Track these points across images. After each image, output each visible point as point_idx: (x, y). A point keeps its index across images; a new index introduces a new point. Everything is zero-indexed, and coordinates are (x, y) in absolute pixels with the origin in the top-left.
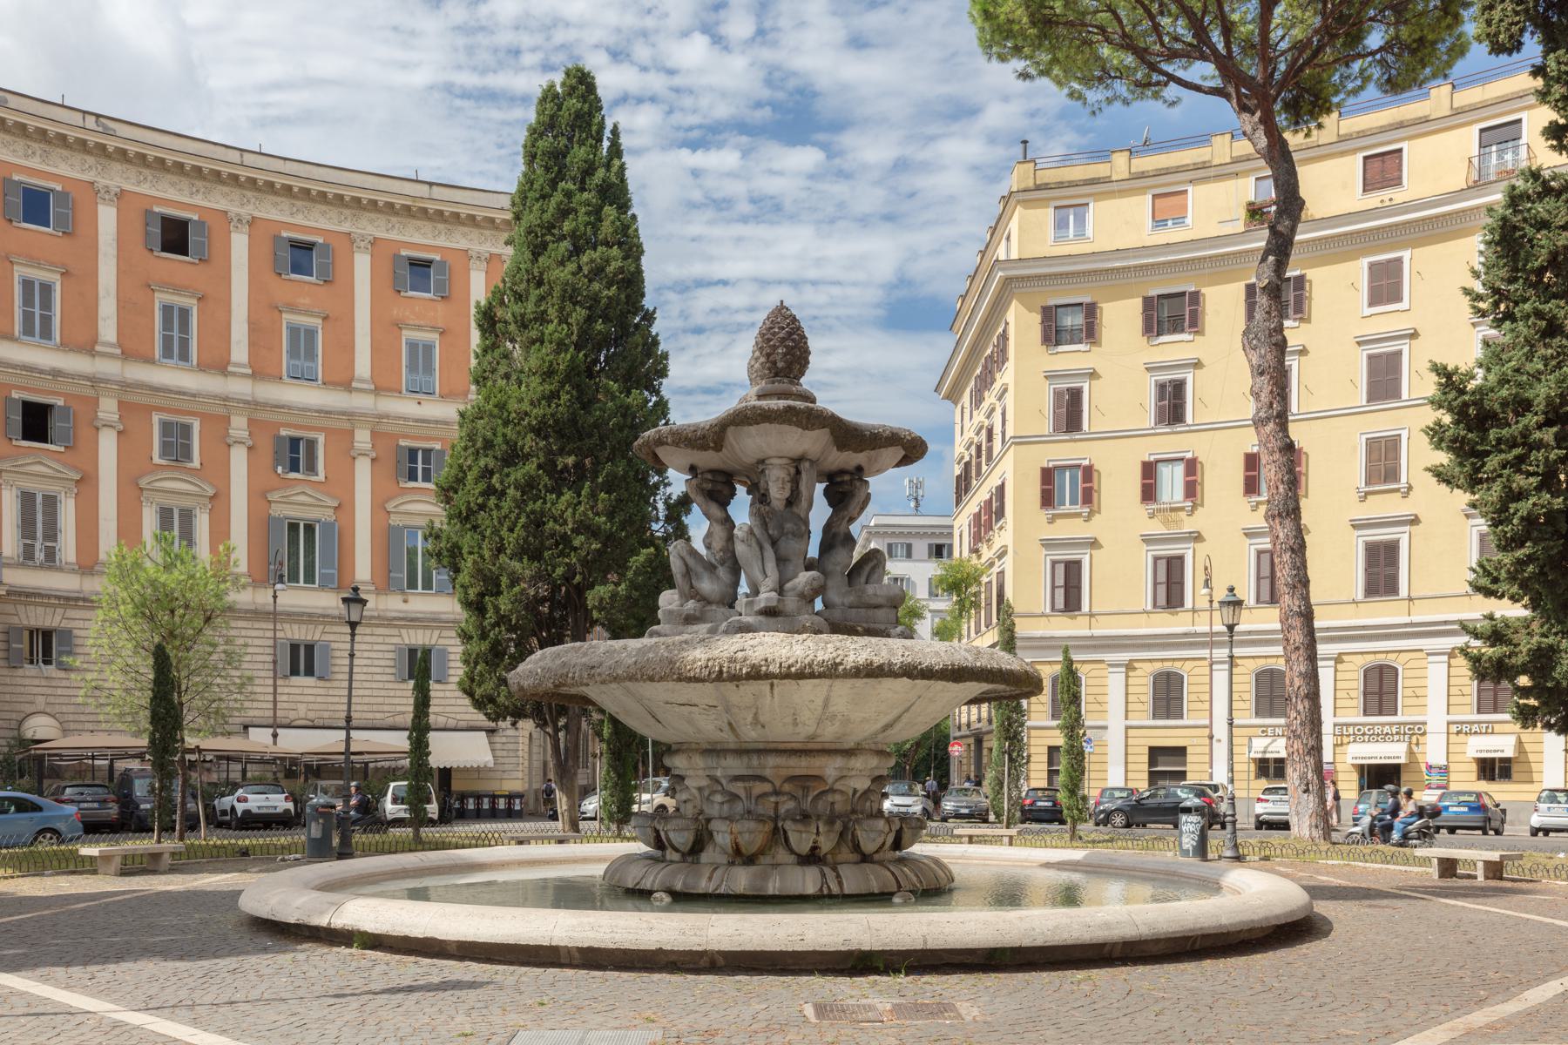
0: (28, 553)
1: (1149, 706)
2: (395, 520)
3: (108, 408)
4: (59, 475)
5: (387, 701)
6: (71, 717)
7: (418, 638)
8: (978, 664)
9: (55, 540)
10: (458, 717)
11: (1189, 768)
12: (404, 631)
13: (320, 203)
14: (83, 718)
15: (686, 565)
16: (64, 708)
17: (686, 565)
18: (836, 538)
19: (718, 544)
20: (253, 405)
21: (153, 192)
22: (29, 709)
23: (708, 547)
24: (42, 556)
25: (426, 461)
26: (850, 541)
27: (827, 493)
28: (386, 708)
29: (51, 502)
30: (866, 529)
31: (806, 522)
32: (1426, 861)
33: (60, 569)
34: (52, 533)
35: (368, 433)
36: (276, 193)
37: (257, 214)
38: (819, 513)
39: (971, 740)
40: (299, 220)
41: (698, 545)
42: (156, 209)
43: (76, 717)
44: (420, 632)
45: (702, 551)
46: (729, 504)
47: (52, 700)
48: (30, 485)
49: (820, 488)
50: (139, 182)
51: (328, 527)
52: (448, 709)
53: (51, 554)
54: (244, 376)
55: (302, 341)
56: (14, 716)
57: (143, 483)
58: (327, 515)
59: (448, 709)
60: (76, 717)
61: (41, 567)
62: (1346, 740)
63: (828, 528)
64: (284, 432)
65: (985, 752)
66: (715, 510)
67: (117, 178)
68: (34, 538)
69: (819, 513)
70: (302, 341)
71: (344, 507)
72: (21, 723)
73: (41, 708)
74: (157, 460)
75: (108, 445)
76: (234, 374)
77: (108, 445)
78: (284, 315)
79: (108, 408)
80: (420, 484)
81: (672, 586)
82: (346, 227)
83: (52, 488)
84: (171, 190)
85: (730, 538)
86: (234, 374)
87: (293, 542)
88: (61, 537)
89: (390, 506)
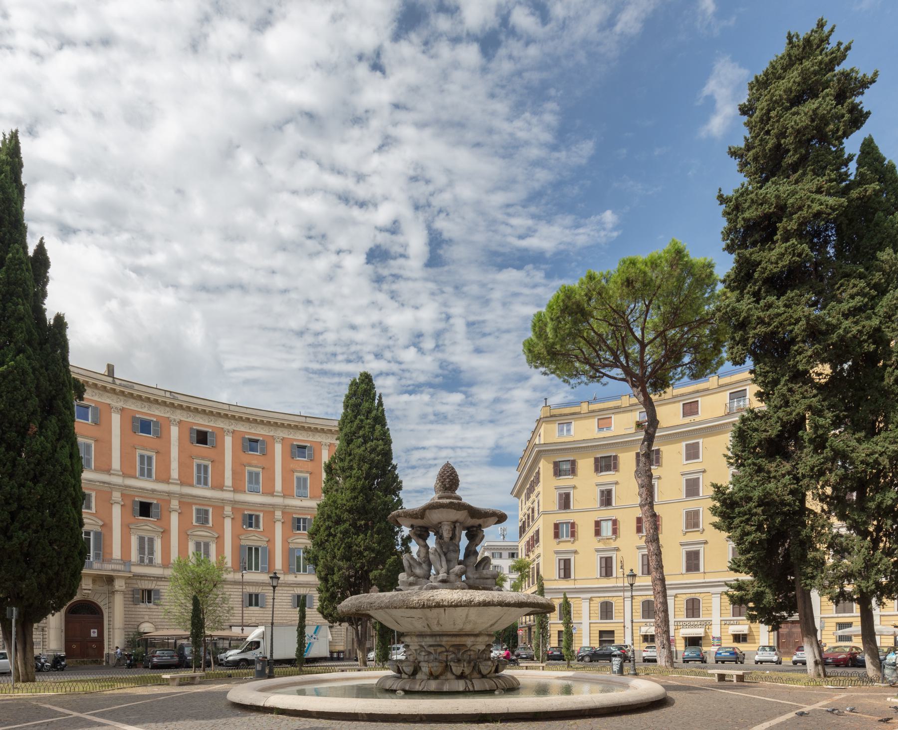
0: (142, 560)
2: (291, 546)
3: (175, 504)
7: (301, 591)
11: (615, 639)
12: (295, 589)
14: (164, 624)
18: (471, 552)
19: (422, 555)
20: (182, 495)
22: (142, 620)
23: (419, 556)
27: (467, 535)
29: (151, 541)
30: (482, 551)
31: (458, 546)
33: (155, 566)
34: (151, 552)
38: (464, 542)
39: (527, 629)
40: (252, 431)
44: (302, 589)
45: (415, 556)
48: (143, 534)
49: (464, 533)
51: (264, 549)
53: (151, 560)
58: (264, 544)
61: (147, 565)
63: (467, 548)
66: (421, 542)
69: (464, 542)
70: (254, 478)
71: (271, 541)
72: (138, 626)
75: (174, 519)
77: (174, 519)
79: (175, 504)
81: (404, 571)
82: (271, 434)
83: (151, 535)
85: (427, 553)
88: (155, 554)
89: (290, 540)
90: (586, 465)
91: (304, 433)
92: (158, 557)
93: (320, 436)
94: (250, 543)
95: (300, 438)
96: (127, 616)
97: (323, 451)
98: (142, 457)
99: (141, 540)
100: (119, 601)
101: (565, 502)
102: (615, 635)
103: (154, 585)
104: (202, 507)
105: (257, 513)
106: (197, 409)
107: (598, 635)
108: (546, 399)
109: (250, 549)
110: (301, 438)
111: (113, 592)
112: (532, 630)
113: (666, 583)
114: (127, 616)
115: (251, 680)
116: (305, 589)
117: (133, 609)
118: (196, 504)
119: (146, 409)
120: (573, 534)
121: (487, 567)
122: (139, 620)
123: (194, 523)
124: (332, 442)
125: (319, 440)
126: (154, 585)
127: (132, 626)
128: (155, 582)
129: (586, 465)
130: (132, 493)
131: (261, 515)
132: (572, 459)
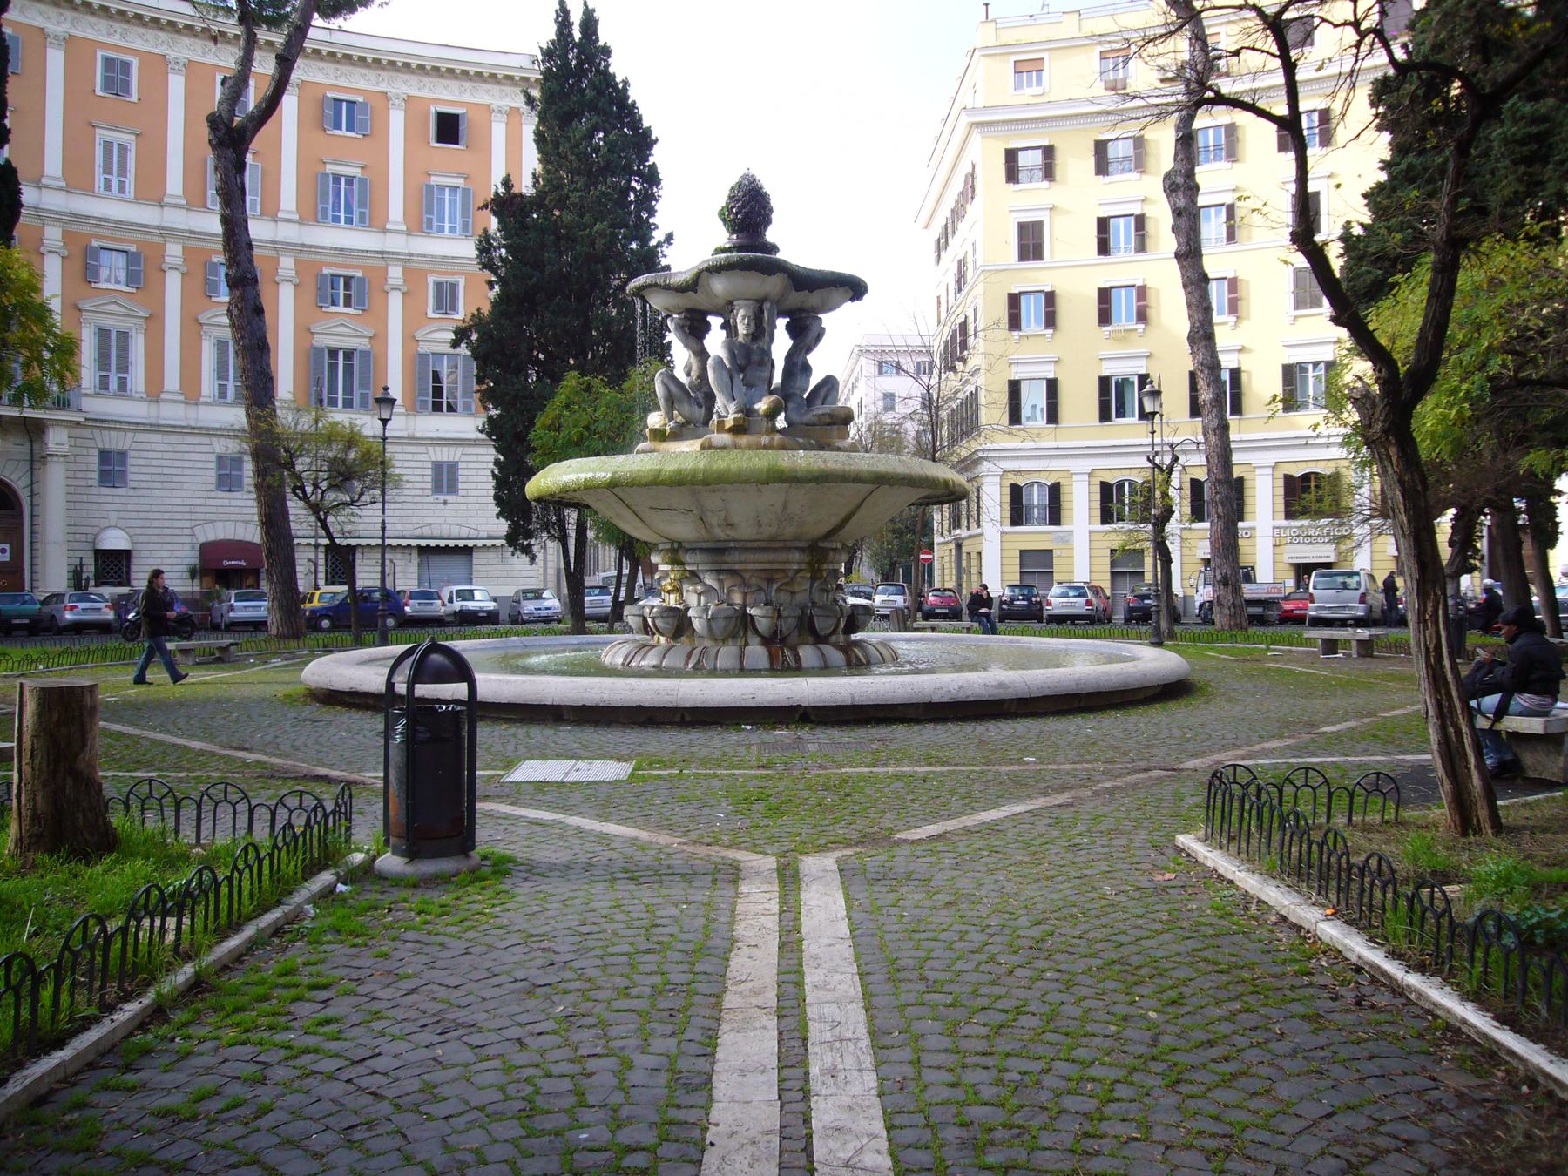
0: (104, 383)
1: (1283, 515)
2: (424, 348)
3: (395, 274)
4: (352, 332)
5: (416, 513)
6: (139, 531)
7: (445, 455)
8: (715, 467)
9: (127, 372)
10: (480, 528)
11: (1055, 569)
12: (430, 449)
13: (361, 67)
14: (150, 531)
15: (669, 391)
16: (133, 523)
17: (669, 391)
18: (797, 366)
19: (694, 373)
20: (302, 248)
21: (215, 62)
22: (104, 523)
23: (688, 374)
24: (115, 387)
25: (347, 286)
26: (807, 369)
27: (789, 328)
28: (415, 520)
29: (124, 337)
30: (821, 363)
31: (768, 353)
32: (1310, 642)
33: (131, 398)
34: (124, 366)
35: (180, 247)
36: (144, 25)
37: (74, 32)
38: (781, 344)
39: (952, 546)
40: (342, 82)
41: (680, 374)
42: (329, 95)
43: (143, 531)
44: (445, 449)
45: (684, 379)
46: (704, 337)
47: (122, 515)
48: (106, 322)
49: (782, 323)
50: (109, 34)
51: (365, 355)
52: (470, 520)
53: (122, 384)
54: (60, 189)
55: (115, 158)
56: (89, 530)
57: (203, 318)
58: (360, 344)
59: (470, 520)
60: (143, 531)
61: (115, 396)
62: (1284, 541)
63: (790, 358)
64: (326, 271)
65: (964, 556)
66: (693, 342)
67: (402, 86)
68: (109, 370)
69: (781, 344)
70: (115, 158)
71: (379, 337)
72: (96, 536)
73: (113, 522)
74: (431, 314)
75: (395, 303)
76: (169, 205)
77: (395, 303)
78: (98, 131)
79: (395, 274)
80: (341, 309)
81: (657, 408)
82: (382, 88)
83: (123, 324)
84: (139, 41)
85: (703, 369)
86: (169, 205)
87: (333, 368)
88: (132, 369)
89: (419, 335)
90: (1076, 163)
91: (453, 84)
92: (138, 378)
93: (487, 91)
94: (334, 342)
95: (445, 96)
96: (72, 513)
97: (495, 125)
98: (108, 146)
99: (103, 334)
100: (55, 478)
101: (1031, 243)
102: (1055, 561)
103: (128, 441)
104: (443, 279)
105: (451, 279)
106: (479, 74)
107: (1108, 560)
108: (987, 5)
109: (333, 353)
110: (450, 96)
111: (43, 457)
112: (965, 550)
113: (1232, 437)
114: (72, 513)
115: (320, 656)
116: (452, 449)
117: (85, 498)
118: (433, 272)
119: (468, 94)
120: (1051, 321)
121: (829, 399)
122: (95, 522)
123: (431, 314)
124: (513, 104)
125: (486, 99)
126: (128, 441)
127: (83, 538)
128: (130, 435)
129: (1076, 163)
130: (87, 230)
131: (461, 281)
132: (1046, 143)
